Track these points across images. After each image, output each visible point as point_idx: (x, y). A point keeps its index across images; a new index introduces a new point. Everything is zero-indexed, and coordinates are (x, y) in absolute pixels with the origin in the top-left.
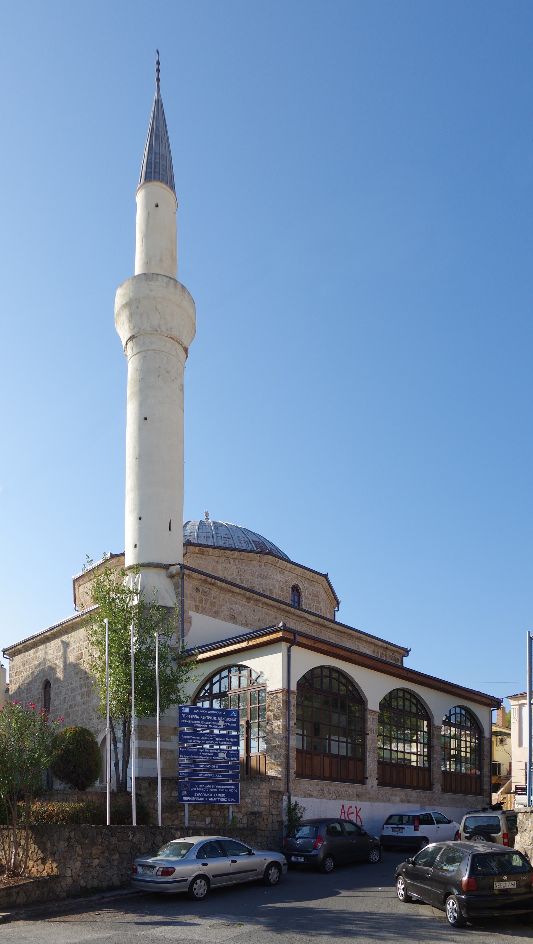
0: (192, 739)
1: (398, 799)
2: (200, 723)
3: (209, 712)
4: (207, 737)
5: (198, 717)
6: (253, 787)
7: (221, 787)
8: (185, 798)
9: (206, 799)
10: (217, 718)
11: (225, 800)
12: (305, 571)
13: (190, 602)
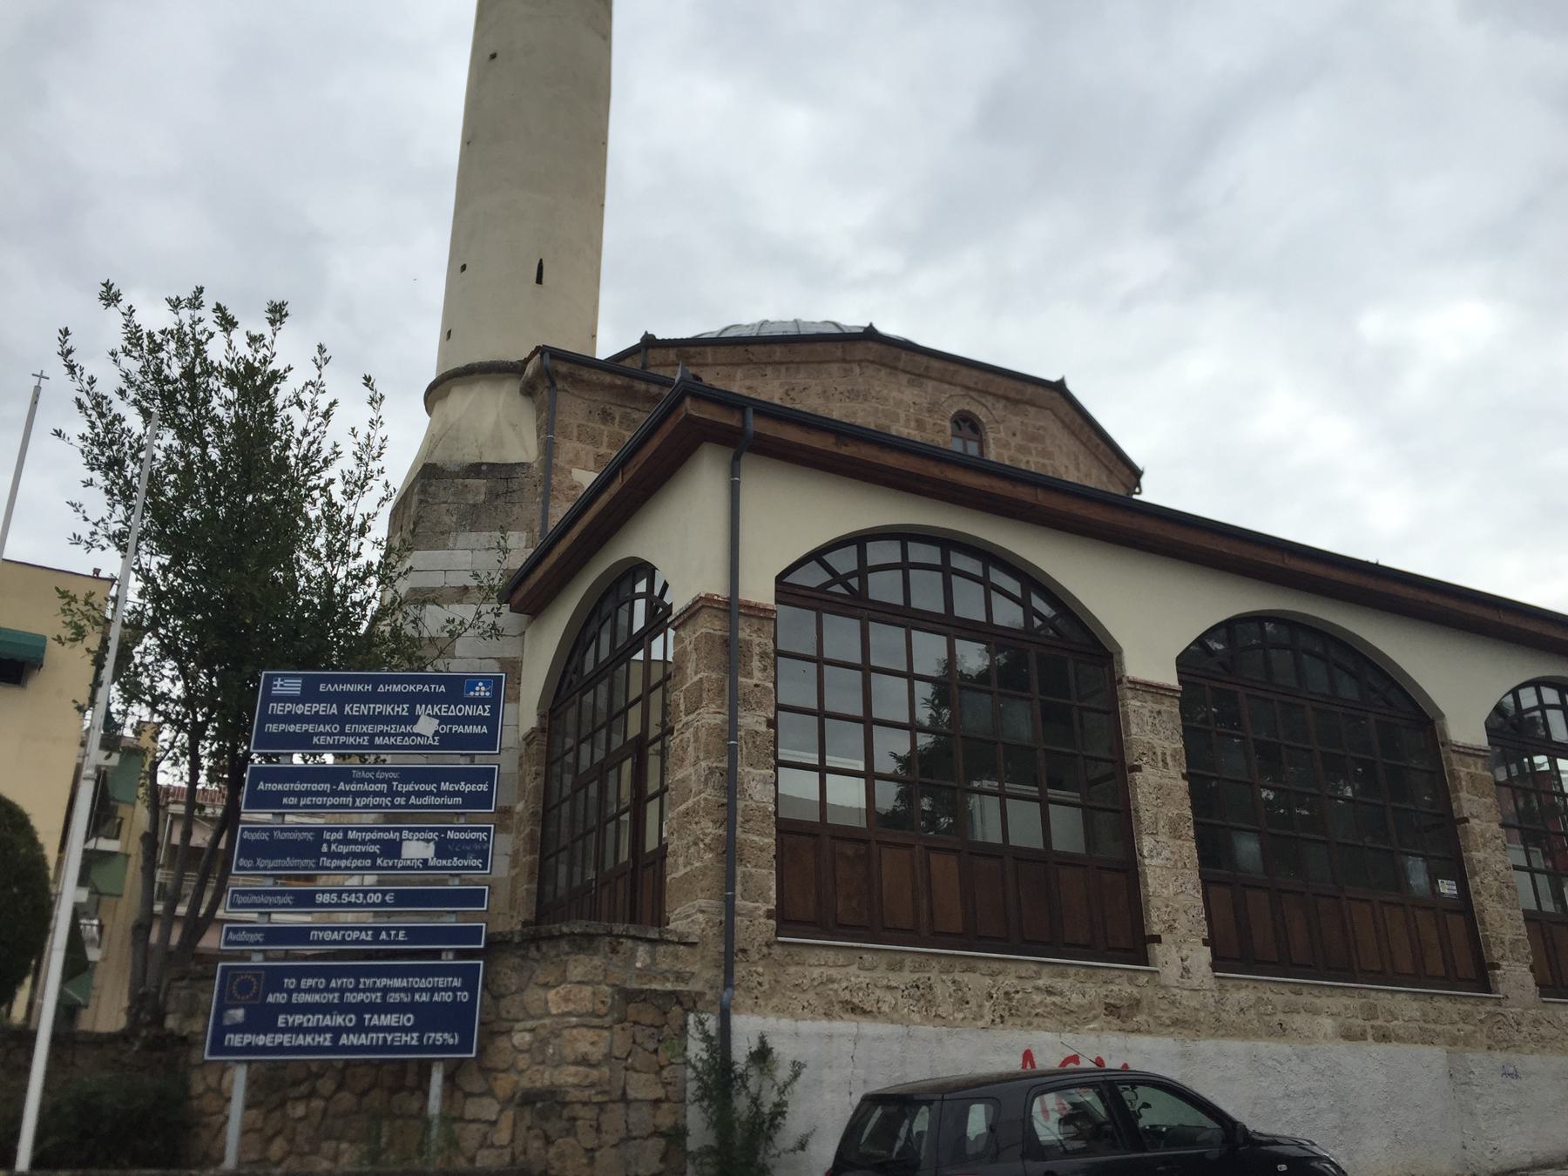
0: (299, 794)
1: (1328, 1024)
2: (342, 733)
3: (381, 689)
4: (362, 781)
5: (334, 710)
6: (541, 980)
7: (397, 983)
8: (235, 1040)
9: (326, 1040)
10: (412, 710)
11: (412, 1039)
12: (991, 376)
13: (579, 445)
